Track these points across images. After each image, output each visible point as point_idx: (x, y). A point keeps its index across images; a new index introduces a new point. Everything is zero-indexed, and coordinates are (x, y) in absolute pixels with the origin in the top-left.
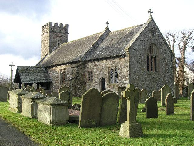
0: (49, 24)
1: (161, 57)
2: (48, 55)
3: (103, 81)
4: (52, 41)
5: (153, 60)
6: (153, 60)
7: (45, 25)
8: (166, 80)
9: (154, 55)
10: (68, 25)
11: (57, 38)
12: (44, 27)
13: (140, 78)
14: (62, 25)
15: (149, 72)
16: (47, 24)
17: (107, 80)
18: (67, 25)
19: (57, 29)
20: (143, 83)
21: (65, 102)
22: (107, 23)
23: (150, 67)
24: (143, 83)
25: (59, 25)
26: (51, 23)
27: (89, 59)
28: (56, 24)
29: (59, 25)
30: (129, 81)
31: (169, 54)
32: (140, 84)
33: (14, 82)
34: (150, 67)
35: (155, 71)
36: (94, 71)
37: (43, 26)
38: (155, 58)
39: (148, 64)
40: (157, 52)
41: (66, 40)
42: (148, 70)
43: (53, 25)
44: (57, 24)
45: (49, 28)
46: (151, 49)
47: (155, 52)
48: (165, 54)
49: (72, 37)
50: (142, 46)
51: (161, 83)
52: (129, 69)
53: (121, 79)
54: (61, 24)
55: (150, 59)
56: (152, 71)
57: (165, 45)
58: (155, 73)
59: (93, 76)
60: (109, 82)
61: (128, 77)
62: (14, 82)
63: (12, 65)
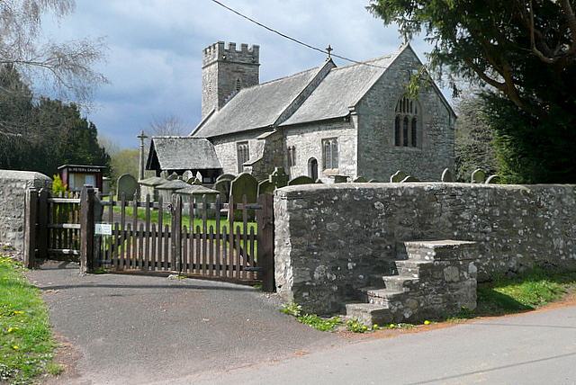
0: (217, 46)
1: (426, 119)
2: (216, 112)
3: (313, 162)
4: (224, 83)
5: (410, 124)
6: (410, 124)
7: (210, 48)
8: (436, 162)
9: (411, 115)
10: (258, 47)
11: (235, 74)
12: (208, 50)
13: (378, 159)
14: (245, 46)
15: (397, 148)
16: (214, 45)
17: (320, 163)
18: (257, 48)
19: (235, 57)
20: (385, 168)
21: (212, 191)
22: (330, 49)
23: (402, 139)
24: (385, 168)
25: (238, 48)
26: (221, 44)
27: (288, 122)
28: (232, 45)
29: (238, 48)
30: (356, 166)
31: (444, 112)
32: (380, 171)
33: (147, 169)
34: (402, 139)
35: (414, 144)
36: (298, 147)
37: (206, 50)
38: (414, 121)
39: (397, 133)
40: (418, 109)
41: (254, 81)
42: (397, 144)
43: (226, 47)
44: (235, 45)
45: (217, 54)
46: (404, 104)
47: (414, 111)
48: (435, 114)
49: (268, 70)
50: (385, 99)
51: (424, 170)
52: (356, 143)
53: (343, 162)
54: (243, 45)
55: (402, 124)
56: (406, 145)
57: (435, 95)
58: (413, 149)
59: (297, 155)
60: (324, 168)
61: (355, 158)
62: (147, 169)
63: (143, 137)
